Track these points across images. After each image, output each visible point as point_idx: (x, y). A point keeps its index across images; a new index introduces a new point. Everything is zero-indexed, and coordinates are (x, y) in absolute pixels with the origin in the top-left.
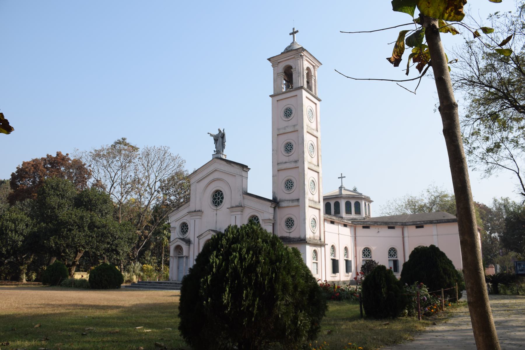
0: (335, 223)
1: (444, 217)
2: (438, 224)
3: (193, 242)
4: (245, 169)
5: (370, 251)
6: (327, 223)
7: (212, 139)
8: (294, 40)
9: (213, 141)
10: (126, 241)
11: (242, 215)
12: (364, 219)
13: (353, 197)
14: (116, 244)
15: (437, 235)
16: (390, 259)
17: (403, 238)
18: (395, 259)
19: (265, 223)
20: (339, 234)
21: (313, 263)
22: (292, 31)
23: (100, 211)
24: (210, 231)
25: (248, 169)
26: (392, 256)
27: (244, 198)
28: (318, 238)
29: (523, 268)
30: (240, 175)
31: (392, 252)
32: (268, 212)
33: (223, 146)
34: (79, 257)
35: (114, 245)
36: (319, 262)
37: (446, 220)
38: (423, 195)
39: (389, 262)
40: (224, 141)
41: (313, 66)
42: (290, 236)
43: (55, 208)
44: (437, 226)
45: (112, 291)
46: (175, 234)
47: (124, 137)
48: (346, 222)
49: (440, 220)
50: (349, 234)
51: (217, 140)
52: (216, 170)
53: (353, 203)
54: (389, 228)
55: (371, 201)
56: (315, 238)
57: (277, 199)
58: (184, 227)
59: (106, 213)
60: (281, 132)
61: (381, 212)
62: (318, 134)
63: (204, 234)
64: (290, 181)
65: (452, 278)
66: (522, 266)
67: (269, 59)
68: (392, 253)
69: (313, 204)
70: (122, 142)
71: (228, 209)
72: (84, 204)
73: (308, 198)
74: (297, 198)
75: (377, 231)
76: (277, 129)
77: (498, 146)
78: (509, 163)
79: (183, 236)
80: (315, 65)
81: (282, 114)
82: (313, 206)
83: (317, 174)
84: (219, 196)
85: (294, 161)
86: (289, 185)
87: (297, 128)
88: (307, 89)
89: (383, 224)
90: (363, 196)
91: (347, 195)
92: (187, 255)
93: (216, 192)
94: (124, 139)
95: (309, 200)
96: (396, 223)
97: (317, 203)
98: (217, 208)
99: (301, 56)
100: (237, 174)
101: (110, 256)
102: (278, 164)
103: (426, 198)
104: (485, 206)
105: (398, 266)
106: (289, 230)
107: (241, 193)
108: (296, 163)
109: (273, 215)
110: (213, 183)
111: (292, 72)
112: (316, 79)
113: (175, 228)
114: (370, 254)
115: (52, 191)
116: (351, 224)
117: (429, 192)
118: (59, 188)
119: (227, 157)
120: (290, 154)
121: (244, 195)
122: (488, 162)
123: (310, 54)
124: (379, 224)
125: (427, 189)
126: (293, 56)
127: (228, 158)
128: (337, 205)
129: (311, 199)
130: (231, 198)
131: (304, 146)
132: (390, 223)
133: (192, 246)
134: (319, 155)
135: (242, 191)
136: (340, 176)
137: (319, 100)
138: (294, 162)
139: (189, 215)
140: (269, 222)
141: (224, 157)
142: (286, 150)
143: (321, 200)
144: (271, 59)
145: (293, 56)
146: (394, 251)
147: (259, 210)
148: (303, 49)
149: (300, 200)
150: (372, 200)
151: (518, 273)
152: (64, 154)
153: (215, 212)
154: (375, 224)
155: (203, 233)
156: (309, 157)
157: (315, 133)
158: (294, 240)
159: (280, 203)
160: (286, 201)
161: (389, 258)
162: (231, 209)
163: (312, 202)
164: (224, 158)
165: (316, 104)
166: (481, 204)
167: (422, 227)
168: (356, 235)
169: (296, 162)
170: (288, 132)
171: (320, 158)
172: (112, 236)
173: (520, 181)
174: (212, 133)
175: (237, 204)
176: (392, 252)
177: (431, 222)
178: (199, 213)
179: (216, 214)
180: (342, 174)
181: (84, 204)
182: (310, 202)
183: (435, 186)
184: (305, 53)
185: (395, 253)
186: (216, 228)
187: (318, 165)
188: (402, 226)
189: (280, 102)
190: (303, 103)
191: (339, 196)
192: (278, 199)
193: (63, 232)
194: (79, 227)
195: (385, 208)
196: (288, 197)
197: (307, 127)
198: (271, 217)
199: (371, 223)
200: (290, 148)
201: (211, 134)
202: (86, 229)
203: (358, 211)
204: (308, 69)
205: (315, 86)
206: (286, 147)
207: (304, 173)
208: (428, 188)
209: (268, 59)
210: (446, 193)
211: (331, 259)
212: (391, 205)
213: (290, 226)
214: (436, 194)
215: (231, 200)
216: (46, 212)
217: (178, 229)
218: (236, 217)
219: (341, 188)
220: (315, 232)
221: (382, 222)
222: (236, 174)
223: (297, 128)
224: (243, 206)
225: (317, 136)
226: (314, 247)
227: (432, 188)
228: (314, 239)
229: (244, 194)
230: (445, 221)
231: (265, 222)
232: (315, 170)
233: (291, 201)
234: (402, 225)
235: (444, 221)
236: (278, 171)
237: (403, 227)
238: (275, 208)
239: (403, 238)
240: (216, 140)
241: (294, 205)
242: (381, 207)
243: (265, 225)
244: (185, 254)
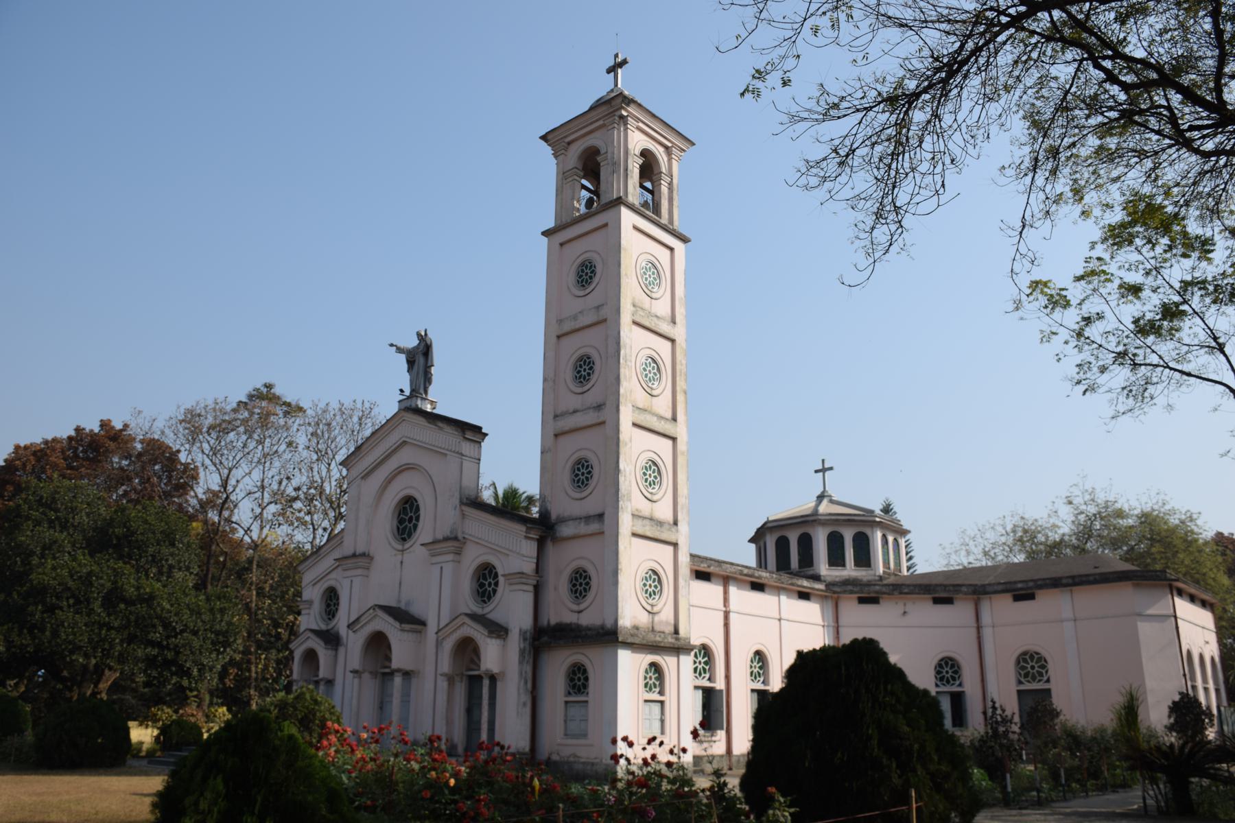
0: (766, 589)
1: (1096, 568)
2: (1074, 588)
4: (469, 435)
5: (959, 667)
6: (788, 597)
7: (402, 358)
9: (406, 366)
11: (459, 562)
12: (881, 578)
13: (849, 520)
15: (1075, 620)
16: (1022, 687)
17: (979, 628)
18: (955, 689)
19: (511, 584)
20: (780, 620)
21: (646, 701)
23: (154, 560)
24: (377, 609)
26: (948, 682)
27: (463, 515)
30: (458, 453)
31: (948, 669)
32: (518, 554)
34: (107, 681)
36: (670, 697)
38: (1056, 512)
40: (429, 364)
41: (666, 148)
42: (580, 622)
43: (32, 553)
44: (1072, 593)
45: (106, 775)
46: (309, 620)
47: (268, 381)
51: (414, 361)
52: (404, 442)
53: (848, 535)
54: (937, 601)
55: (904, 533)
56: (657, 628)
57: (550, 514)
58: (331, 597)
60: (567, 327)
61: (945, 562)
63: (365, 616)
64: (586, 464)
65: (919, 767)
68: (947, 672)
69: (647, 528)
71: (423, 548)
72: (115, 542)
73: (629, 510)
74: (598, 511)
75: (902, 612)
76: (557, 321)
77: (1171, 312)
80: (669, 145)
81: (572, 278)
82: (649, 534)
83: (670, 442)
84: (411, 512)
85: (596, 405)
86: (582, 473)
87: (604, 312)
92: (330, 677)
94: (269, 386)
95: (633, 515)
96: (957, 588)
97: (666, 526)
98: (403, 545)
99: (622, 117)
100: (451, 451)
101: (162, 679)
102: (556, 416)
103: (1063, 521)
107: (457, 502)
108: (599, 410)
109: (535, 561)
111: (598, 164)
112: (675, 181)
113: (310, 603)
117: (1070, 503)
118: (57, 504)
121: (464, 508)
123: (650, 112)
124: (906, 591)
126: (601, 122)
127: (439, 411)
128: (806, 543)
129: (646, 513)
130: (435, 517)
133: (341, 650)
134: (678, 388)
135: (458, 497)
136: (821, 467)
137: (684, 239)
138: (594, 407)
139: (340, 569)
141: (428, 408)
144: (549, 137)
145: (601, 122)
146: (952, 666)
148: (625, 97)
150: (908, 529)
152: (118, 425)
153: (399, 557)
154: (894, 590)
156: (641, 398)
157: (665, 328)
158: (589, 633)
159: (556, 527)
160: (573, 519)
161: (1020, 682)
162: (431, 547)
163: (647, 522)
164: (429, 410)
165: (672, 249)
167: (1031, 597)
168: (840, 624)
169: (599, 407)
170: (581, 325)
172: (167, 625)
174: (401, 345)
175: (447, 533)
177: (1056, 583)
178: (362, 562)
179: (402, 562)
180: (823, 461)
181: (115, 542)
182: (640, 522)
183: (1088, 487)
184: (632, 109)
185: (956, 672)
186: (399, 601)
187: (674, 419)
188: (975, 596)
190: (623, 242)
191: (807, 521)
192: (554, 516)
193: (32, 615)
194: (78, 602)
196: (577, 509)
197: (632, 308)
198: (529, 567)
199: (884, 589)
200: (587, 371)
201: (399, 345)
202: (97, 606)
203: (863, 559)
204: (646, 154)
207: (618, 438)
208: (1069, 495)
210: (1118, 506)
212: (971, 543)
214: (1092, 510)
216: (8, 563)
217: (317, 607)
218: (442, 568)
219: (821, 497)
220: (656, 609)
221: (915, 586)
222: (447, 450)
223: (604, 312)
225: (671, 336)
226: (651, 653)
227: (1080, 494)
228: (653, 630)
229: (466, 504)
233: (583, 520)
235: (1091, 578)
236: (556, 436)
237: (979, 599)
239: (979, 628)
240: (411, 363)
241: (590, 532)
242: (944, 549)
243: (511, 591)
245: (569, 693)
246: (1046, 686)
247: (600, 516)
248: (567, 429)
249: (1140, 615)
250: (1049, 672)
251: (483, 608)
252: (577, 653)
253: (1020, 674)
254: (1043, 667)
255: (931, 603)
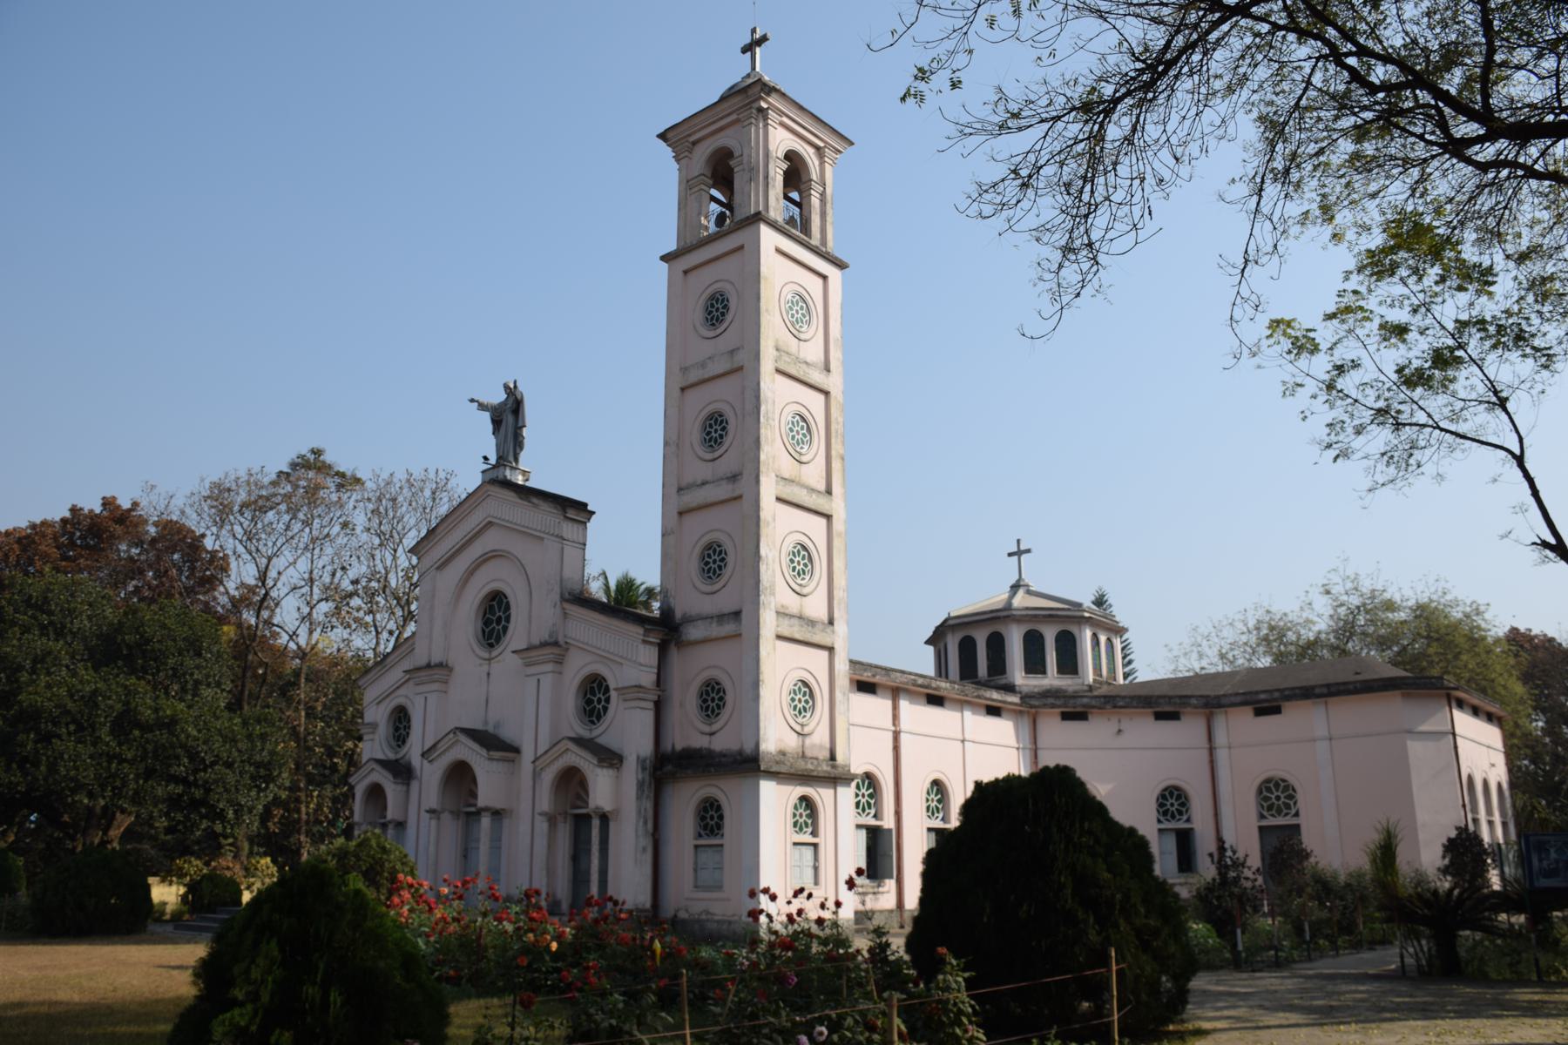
1: (1357, 673)
3: (418, 773)
4: (571, 514)
5: (1186, 798)
8: (754, 68)
9: (490, 427)
10: (246, 772)
11: (560, 673)
12: (1091, 688)
13: (1051, 616)
14: (206, 782)
15: (1331, 739)
16: (1264, 823)
17: (1212, 750)
18: (1182, 825)
19: (625, 700)
20: (963, 741)
22: (748, 40)
24: (458, 733)
25: (583, 514)
26: (1173, 817)
27: (565, 615)
28: (826, 754)
29: (1557, 861)
30: (557, 536)
33: (518, 443)
34: (119, 827)
35: (197, 786)
36: (825, 839)
37: (1358, 685)
38: (1310, 604)
39: (1160, 838)
40: (520, 424)
41: (818, 148)
42: (712, 747)
46: (373, 747)
47: (316, 445)
48: (1000, 701)
49: (1338, 684)
50: (1013, 741)
51: (501, 421)
52: (490, 523)
53: (1050, 635)
54: (1160, 716)
58: (401, 720)
59: (197, 683)
60: (694, 376)
61: (1173, 667)
62: (834, 382)
63: (439, 745)
64: (718, 549)
66: (1553, 855)
67: (662, 136)
69: (796, 629)
70: (313, 463)
71: (515, 656)
72: (125, 652)
75: (1116, 730)
76: (681, 369)
77: (1443, 359)
78: (1494, 426)
79: (397, 753)
81: (699, 315)
82: (798, 636)
85: (729, 475)
86: (713, 561)
87: (741, 358)
88: (787, 227)
89: (1135, 704)
90: (1085, 611)
91: (1027, 609)
92: (399, 817)
93: (493, 599)
94: (317, 452)
95: (778, 613)
96: (1184, 700)
97: (820, 627)
98: (490, 652)
99: (760, 110)
100: (548, 534)
102: (680, 489)
104: (1552, 640)
105: (1195, 852)
106: (710, 725)
107: (557, 597)
108: (734, 481)
109: (656, 671)
110: (484, 568)
112: (829, 191)
113: (374, 726)
114: (1184, 810)
115: (25, 614)
116: (1020, 705)
117: (1328, 592)
119: (532, 476)
120: (717, 454)
121: (567, 606)
122: (1398, 424)
124: (1121, 704)
125: (1324, 585)
126: (734, 117)
127: (533, 483)
128: (997, 645)
131: (762, 419)
132: (1162, 701)
133: (414, 785)
135: (559, 591)
136: (1015, 549)
137: (840, 265)
138: (727, 478)
140: (636, 695)
141: (520, 480)
142: (707, 438)
143: (836, 615)
144: (669, 135)
145: (734, 117)
146: (1179, 797)
147: (612, 657)
149: (744, 615)
151: (1536, 884)
152: (125, 504)
153: (485, 668)
154: (1105, 703)
155: (439, 741)
156: (787, 466)
158: (723, 760)
159: (681, 628)
161: (1262, 817)
163: (795, 621)
164: (520, 483)
165: (824, 278)
166: (1536, 636)
167: (1276, 710)
169: (734, 478)
170: (711, 374)
171: (836, 465)
172: (193, 756)
173: (1529, 492)
174: (485, 400)
175: (545, 637)
176: (1173, 801)
177: (1307, 693)
179: (489, 674)
180: (1018, 541)
181: (125, 652)
183: (1350, 572)
185: (1183, 805)
187: (829, 492)
188: (1207, 711)
189: (692, 276)
190: (763, 269)
192: (678, 615)
193: (23, 745)
194: (80, 728)
195: (1186, 654)
196: (707, 606)
197: (775, 353)
198: (648, 678)
199: (1094, 702)
201: (481, 400)
202: (104, 733)
203: (1069, 663)
205: (823, 215)
206: (708, 429)
207: (758, 517)
208: (1327, 582)
209: (659, 136)
211: (929, 830)
213: (713, 711)
214: (1355, 601)
215: (530, 622)
217: (383, 730)
218: (539, 680)
221: (1132, 698)
222: (544, 532)
223: (741, 358)
224: (562, 642)
225: (825, 387)
226: (800, 785)
228: (803, 756)
229: (567, 601)
230: (1355, 687)
231: (627, 696)
232: (813, 507)
234: (1206, 705)
235: (1351, 687)
238: (663, 649)
239: (1212, 750)
240: (497, 423)
242: (1170, 650)
243: (625, 709)
244: (391, 814)
245: (700, 835)
246: (1294, 821)
247: (737, 614)
248: (694, 505)
249: (1410, 732)
250: (1299, 804)
251: (591, 730)
252: (710, 785)
253: (1262, 806)
254: (1291, 797)
255: (1152, 718)
